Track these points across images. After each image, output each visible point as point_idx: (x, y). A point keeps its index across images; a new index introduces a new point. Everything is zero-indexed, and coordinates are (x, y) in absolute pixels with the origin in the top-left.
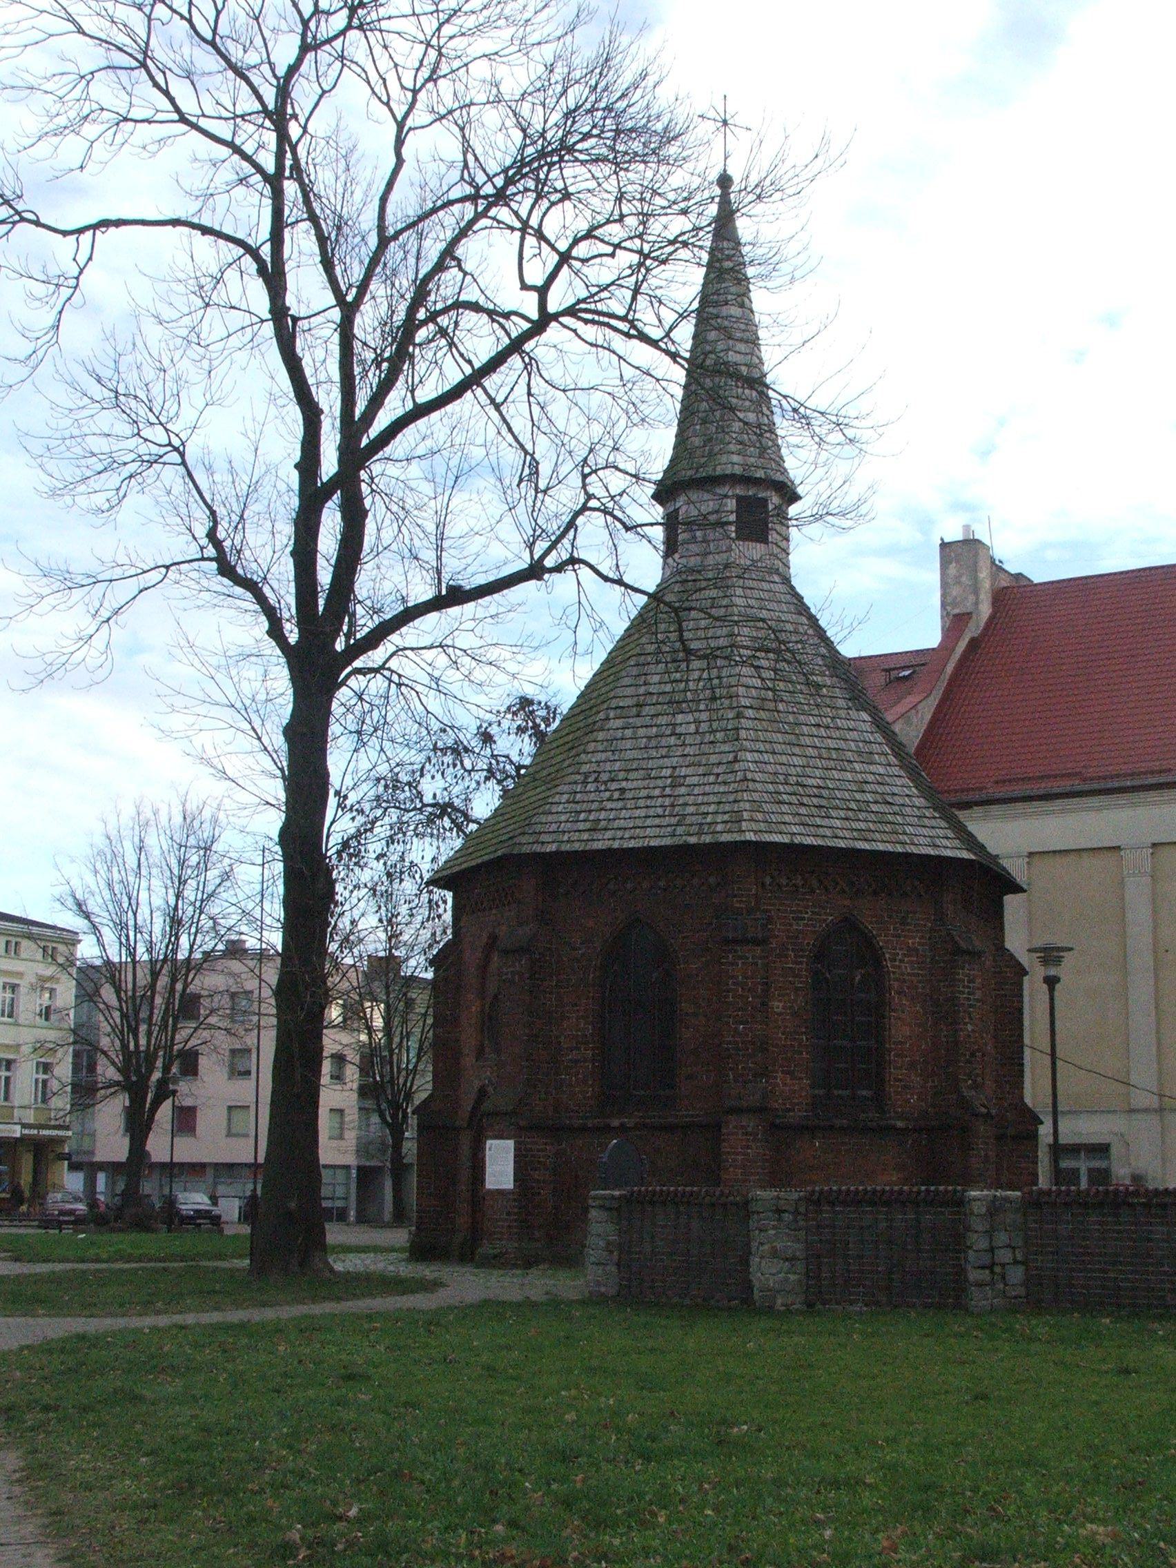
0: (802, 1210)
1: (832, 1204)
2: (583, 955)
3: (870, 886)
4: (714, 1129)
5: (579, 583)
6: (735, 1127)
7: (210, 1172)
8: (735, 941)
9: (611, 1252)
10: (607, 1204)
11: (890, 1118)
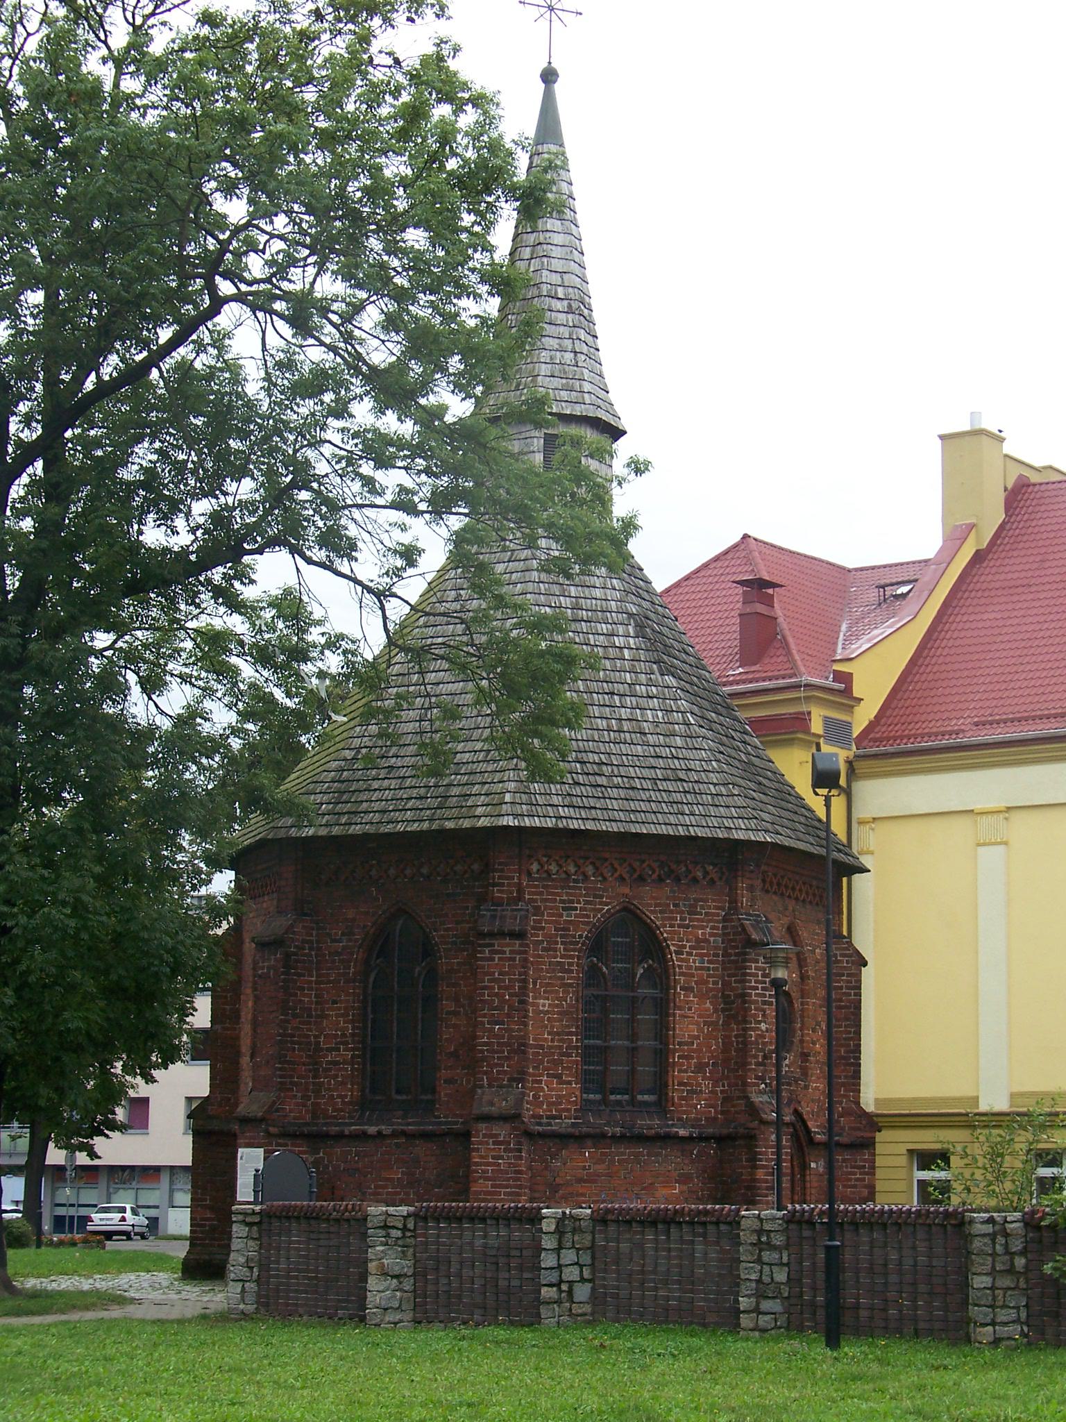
0: (411, 1225)
1: (438, 1220)
2: (344, 948)
3: (654, 871)
4: (465, 1136)
5: (297, 569)
6: (485, 1136)
7: (165, 1178)
8: (491, 935)
9: (251, 1268)
10: (249, 1219)
11: (673, 1125)
